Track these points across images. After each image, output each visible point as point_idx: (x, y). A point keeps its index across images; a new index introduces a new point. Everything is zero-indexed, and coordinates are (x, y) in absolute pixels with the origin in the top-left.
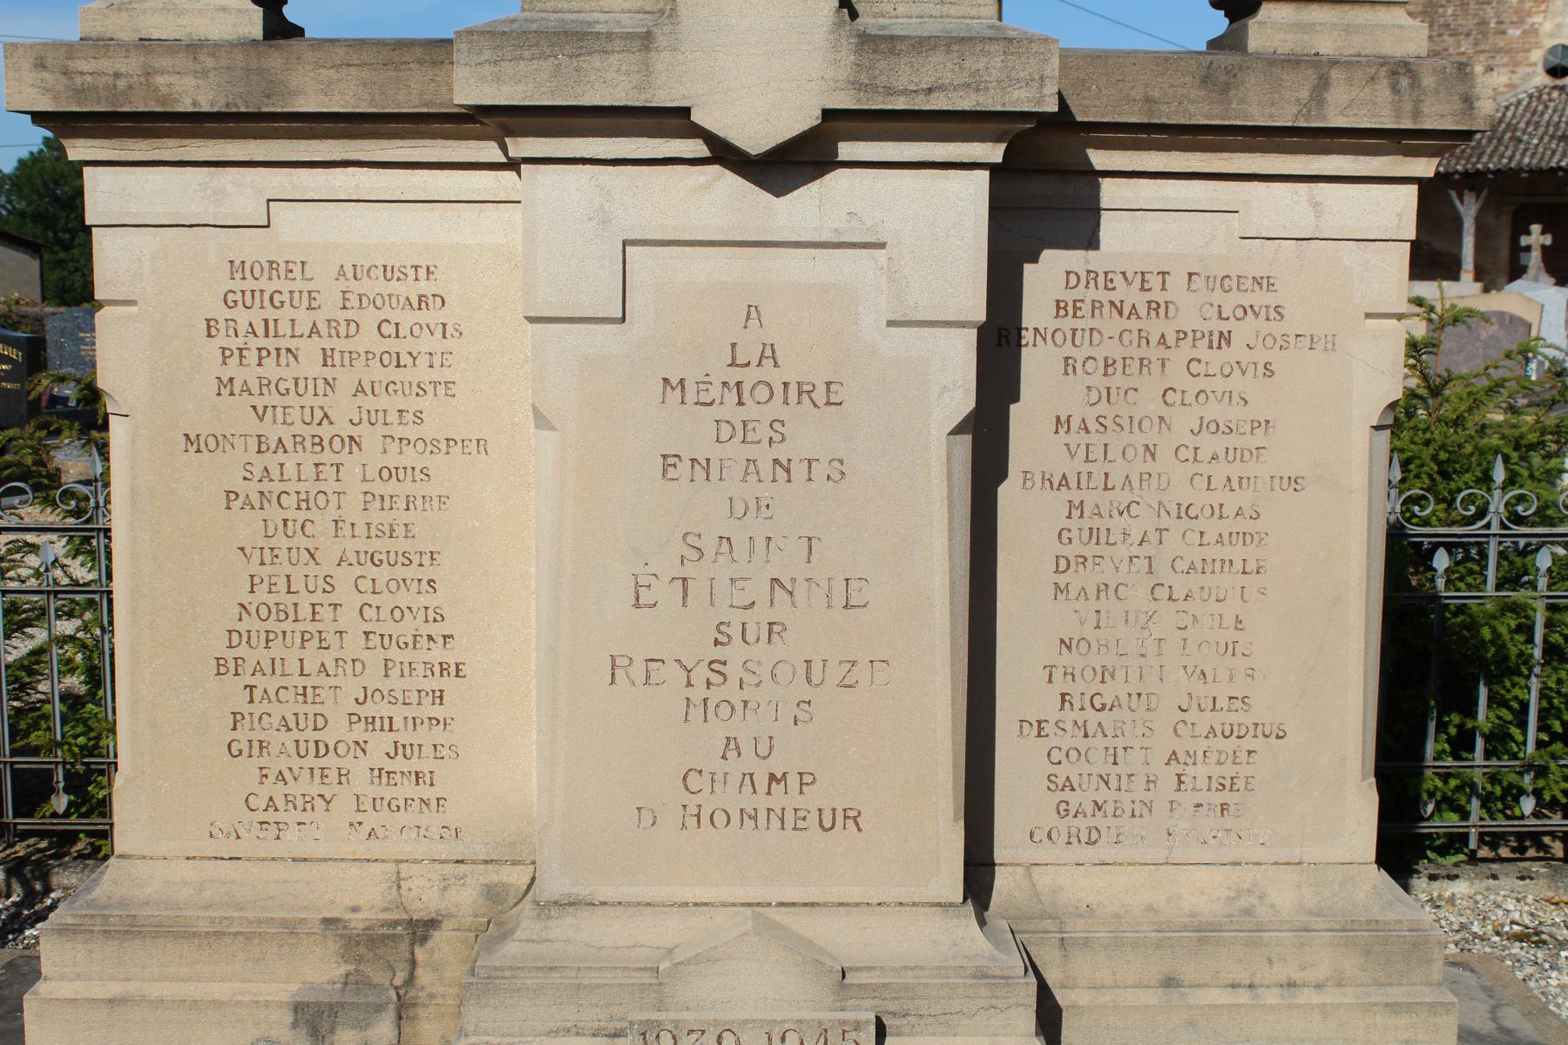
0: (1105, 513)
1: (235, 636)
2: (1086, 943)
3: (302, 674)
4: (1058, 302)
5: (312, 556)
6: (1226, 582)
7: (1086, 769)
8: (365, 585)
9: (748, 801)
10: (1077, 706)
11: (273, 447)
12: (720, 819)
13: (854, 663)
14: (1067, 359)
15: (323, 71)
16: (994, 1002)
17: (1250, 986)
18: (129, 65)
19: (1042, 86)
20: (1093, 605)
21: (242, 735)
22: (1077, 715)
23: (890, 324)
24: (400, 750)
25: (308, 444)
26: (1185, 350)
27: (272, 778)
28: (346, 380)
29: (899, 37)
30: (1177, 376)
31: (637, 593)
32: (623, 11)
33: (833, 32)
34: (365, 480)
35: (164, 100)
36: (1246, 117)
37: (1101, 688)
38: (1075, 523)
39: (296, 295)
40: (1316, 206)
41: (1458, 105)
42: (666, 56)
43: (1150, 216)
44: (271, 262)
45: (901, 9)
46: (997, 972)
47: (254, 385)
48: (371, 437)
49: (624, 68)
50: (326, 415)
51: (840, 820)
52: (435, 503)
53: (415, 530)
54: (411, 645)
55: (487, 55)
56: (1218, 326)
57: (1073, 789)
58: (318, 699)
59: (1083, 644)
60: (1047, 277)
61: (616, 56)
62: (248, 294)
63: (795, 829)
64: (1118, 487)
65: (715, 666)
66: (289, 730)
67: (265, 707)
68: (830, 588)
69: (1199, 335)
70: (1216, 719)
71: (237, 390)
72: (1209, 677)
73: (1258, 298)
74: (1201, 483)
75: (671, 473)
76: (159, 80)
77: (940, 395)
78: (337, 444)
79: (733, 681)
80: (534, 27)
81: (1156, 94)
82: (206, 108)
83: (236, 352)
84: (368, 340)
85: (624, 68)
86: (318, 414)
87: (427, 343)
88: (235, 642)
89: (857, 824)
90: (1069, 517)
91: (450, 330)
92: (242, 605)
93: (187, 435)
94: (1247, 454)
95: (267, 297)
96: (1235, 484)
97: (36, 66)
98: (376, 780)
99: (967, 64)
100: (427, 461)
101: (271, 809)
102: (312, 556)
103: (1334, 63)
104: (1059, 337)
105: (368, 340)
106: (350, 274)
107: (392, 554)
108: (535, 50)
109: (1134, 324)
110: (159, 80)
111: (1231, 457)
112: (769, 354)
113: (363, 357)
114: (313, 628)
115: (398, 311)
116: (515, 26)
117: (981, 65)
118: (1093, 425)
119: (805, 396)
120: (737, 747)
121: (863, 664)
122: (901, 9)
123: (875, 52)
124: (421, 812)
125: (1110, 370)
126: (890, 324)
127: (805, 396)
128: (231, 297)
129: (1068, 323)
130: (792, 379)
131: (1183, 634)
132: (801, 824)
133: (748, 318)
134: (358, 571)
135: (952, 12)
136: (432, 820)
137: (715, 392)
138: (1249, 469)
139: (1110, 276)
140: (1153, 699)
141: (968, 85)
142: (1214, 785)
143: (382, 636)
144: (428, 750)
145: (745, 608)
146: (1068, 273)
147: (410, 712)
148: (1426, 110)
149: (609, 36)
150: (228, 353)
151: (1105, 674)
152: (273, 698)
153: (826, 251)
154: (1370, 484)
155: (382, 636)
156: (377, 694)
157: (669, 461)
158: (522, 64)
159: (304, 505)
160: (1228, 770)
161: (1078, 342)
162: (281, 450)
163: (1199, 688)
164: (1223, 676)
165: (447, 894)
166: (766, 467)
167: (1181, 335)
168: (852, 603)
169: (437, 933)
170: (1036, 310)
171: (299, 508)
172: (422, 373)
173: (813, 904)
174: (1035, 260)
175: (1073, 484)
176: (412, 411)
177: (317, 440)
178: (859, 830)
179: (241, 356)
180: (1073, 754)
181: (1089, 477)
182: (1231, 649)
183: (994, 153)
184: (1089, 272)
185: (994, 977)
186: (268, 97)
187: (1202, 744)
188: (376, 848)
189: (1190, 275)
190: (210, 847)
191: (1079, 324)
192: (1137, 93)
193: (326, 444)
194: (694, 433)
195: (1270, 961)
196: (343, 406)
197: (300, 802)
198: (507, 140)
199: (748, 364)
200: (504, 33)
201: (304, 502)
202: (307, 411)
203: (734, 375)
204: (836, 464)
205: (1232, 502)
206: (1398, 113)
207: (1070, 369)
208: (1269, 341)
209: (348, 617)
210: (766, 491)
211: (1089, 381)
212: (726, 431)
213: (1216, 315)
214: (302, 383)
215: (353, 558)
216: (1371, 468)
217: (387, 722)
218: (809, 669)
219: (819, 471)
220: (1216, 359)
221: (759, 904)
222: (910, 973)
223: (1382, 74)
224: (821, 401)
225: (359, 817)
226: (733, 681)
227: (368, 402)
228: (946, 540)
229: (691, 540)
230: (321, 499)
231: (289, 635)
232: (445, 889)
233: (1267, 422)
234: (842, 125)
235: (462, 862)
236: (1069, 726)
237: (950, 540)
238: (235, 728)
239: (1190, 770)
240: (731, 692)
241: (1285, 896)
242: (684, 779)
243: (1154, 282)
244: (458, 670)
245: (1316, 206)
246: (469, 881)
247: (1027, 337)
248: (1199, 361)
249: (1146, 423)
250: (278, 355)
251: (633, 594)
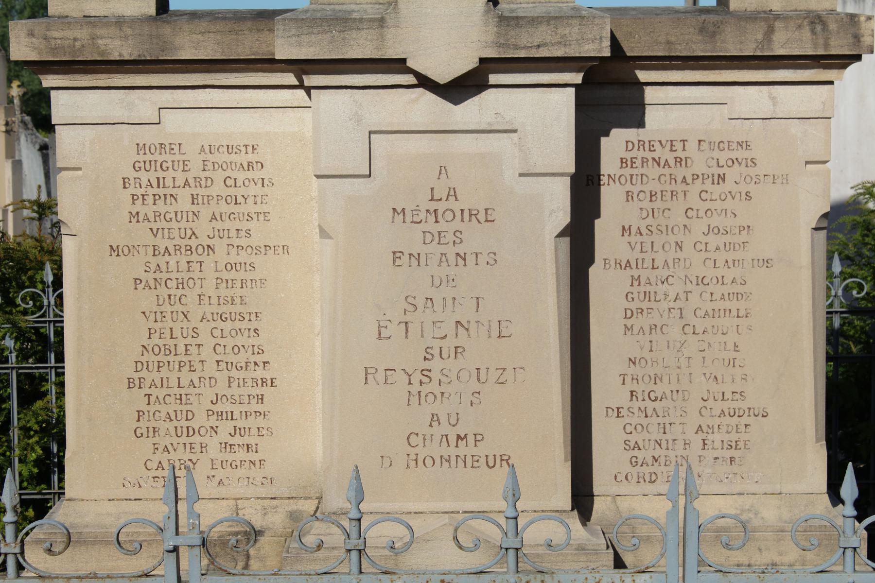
0: (653, 283)
1: (139, 365)
4: (622, 159)
5: (186, 316)
7: (647, 436)
8: (217, 333)
9: (445, 451)
10: (640, 398)
11: (162, 252)
12: (429, 462)
13: (504, 370)
14: (628, 192)
15: (194, 35)
17: (749, 566)
18: (82, 34)
19: (601, 42)
20: (648, 337)
21: (143, 424)
22: (640, 404)
23: (521, 175)
24: (238, 431)
25: (183, 250)
26: (698, 186)
27: (161, 450)
28: (206, 213)
29: (521, 17)
30: (693, 200)
31: (379, 331)
32: (367, 4)
33: (484, 16)
34: (216, 271)
35: (103, 53)
36: (726, 51)
37: (654, 388)
38: (635, 289)
39: (176, 163)
40: (774, 100)
41: (851, 40)
42: (392, 30)
43: (673, 108)
44: (161, 144)
46: (590, 547)
47: (151, 216)
48: (220, 246)
50: (194, 233)
53: (247, 300)
54: (244, 368)
55: (293, 31)
56: (718, 171)
57: (640, 449)
58: (188, 402)
59: (643, 362)
60: (615, 145)
61: (365, 31)
62: (148, 163)
63: (472, 467)
64: (661, 267)
65: (425, 373)
66: (171, 420)
67: (157, 407)
69: (706, 176)
70: (725, 406)
71: (141, 219)
72: (720, 380)
73: (741, 154)
74: (710, 263)
75: (398, 262)
76: (100, 42)
77: (550, 214)
80: (319, 15)
81: (673, 39)
82: (127, 58)
83: (141, 197)
84: (218, 189)
86: (189, 232)
87: (253, 190)
90: (632, 285)
92: (144, 346)
93: (111, 246)
95: (158, 165)
96: (730, 264)
97: (28, 35)
98: (223, 450)
99: (559, 31)
100: (253, 259)
101: (160, 469)
102: (186, 316)
103: (777, 17)
104: (623, 180)
106: (207, 151)
107: (233, 314)
108: (320, 29)
109: (667, 171)
110: (100, 42)
111: (727, 248)
112: (453, 194)
113: (215, 198)
114: (186, 359)
115: (236, 172)
116: (308, 15)
117: (567, 32)
118: (644, 231)
119: (473, 217)
120: (438, 420)
123: (508, 25)
126: (521, 175)
127: (473, 217)
128: (137, 165)
129: (628, 171)
131: (703, 354)
132: (476, 464)
133: (440, 173)
134: (213, 324)
136: (257, 474)
137: (422, 216)
138: (738, 255)
139: (652, 143)
140: (686, 393)
141: (560, 43)
142: (726, 446)
143: (227, 363)
144: (254, 431)
145: (442, 338)
146: (627, 142)
147: (244, 408)
148: (832, 43)
149: (361, 20)
150: (135, 197)
152: (162, 401)
154: (813, 263)
155: (227, 363)
157: (396, 255)
158: (313, 36)
159: (180, 286)
160: (734, 437)
161: (634, 182)
162: (167, 254)
163: (716, 388)
164: (728, 379)
165: (266, 517)
166: (452, 258)
167: (695, 177)
168: (502, 334)
169: (262, 538)
170: (609, 164)
174: (607, 135)
176: (244, 230)
177: (188, 248)
179: (144, 199)
180: (639, 428)
182: (732, 362)
183: (577, 78)
184: (639, 141)
186: (163, 51)
187: (717, 421)
188: (223, 492)
189: (700, 141)
190: (122, 493)
191: (634, 172)
192: (662, 39)
193: (193, 250)
194: (411, 239)
195: (760, 550)
196: (203, 228)
198: (304, 77)
199: (441, 200)
200: (303, 19)
201: (181, 284)
202: (183, 231)
203: (433, 206)
204: (492, 255)
206: (815, 46)
207: (630, 198)
208: (748, 179)
209: (206, 352)
210: (452, 271)
211: (641, 205)
212: (429, 237)
213: (716, 164)
215: (210, 317)
216: (813, 253)
217: (230, 414)
218: (478, 373)
219: (482, 259)
220: (716, 190)
221: (452, 512)
223: (805, 23)
224: (482, 219)
225: (213, 473)
227: (219, 225)
229: (410, 300)
230: (191, 282)
231: (171, 363)
232: (265, 514)
233: (749, 227)
235: (274, 498)
236: (636, 410)
238: (139, 420)
239: (710, 437)
240: (434, 387)
241: (770, 513)
242: (408, 439)
243: (679, 146)
244: (272, 382)
245: (774, 100)
246: (279, 510)
247: (604, 180)
248: (707, 192)
249: (676, 229)
250: (165, 198)
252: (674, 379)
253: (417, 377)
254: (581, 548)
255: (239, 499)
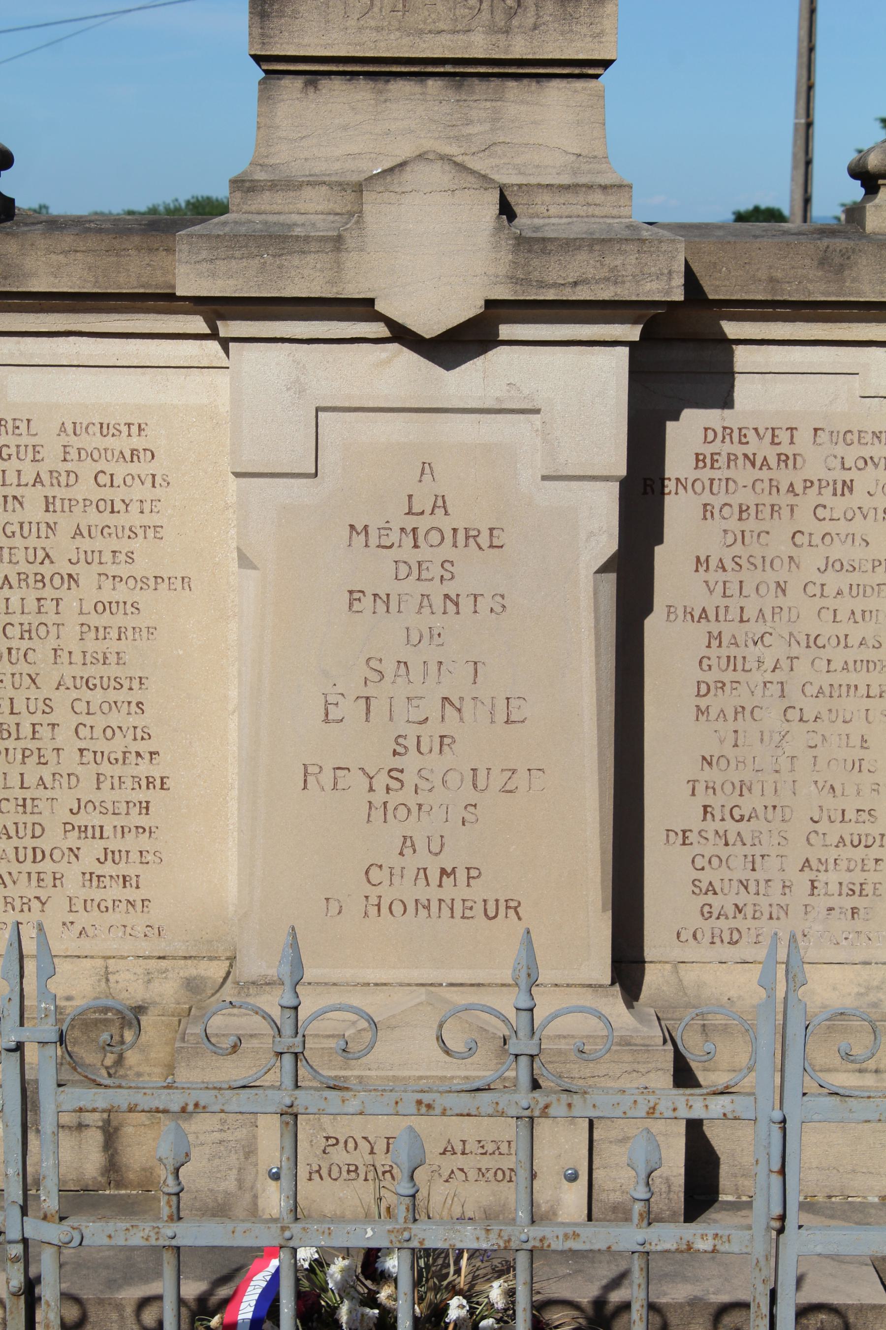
2: (725, 1029)
3: (22, 787)
4: (697, 455)
5: (33, 681)
6: (851, 705)
8: (81, 707)
9: (422, 892)
10: (718, 817)
12: (398, 908)
13: (514, 771)
14: (705, 505)
15: (53, 256)
16: (636, 1066)
20: (731, 725)
23: (545, 478)
25: (31, 580)
26: (813, 497)
28: (66, 524)
30: (804, 519)
33: (494, 235)
34: (81, 613)
36: (859, 294)
37: (739, 801)
38: (714, 652)
39: (22, 449)
43: (778, 379)
45: (553, 210)
48: (87, 575)
49: (318, 266)
50: (47, 556)
51: (502, 909)
52: (144, 633)
53: (126, 658)
54: (121, 761)
55: (204, 254)
57: (715, 893)
58: (36, 810)
59: (723, 761)
60: (687, 434)
61: (313, 256)
63: (463, 917)
64: (753, 620)
65: (393, 774)
66: (10, 837)
68: (493, 705)
69: (824, 484)
70: (846, 830)
72: (838, 791)
74: (828, 615)
78: (57, 581)
79: (409, 787)
80: (243, 230)
81: (779, 275)
84: (85, 489)
85: (318, 266)
86: (41, 554)
87: (138, 492)
88: (403, 573)
89: (517, 913)
90: (709, 646)
91: (158, 480)
94: (869, 590)
96: (858, 616)
98: (87, 883)
99: (607, 261)
100: (137, 596)
102: (33, 681)
104: (698, 487)
105: (85, 489)
107: (105, 679)
109: (765, 474)
111: (854, 593)
112: (441, 504)
113: (81, 504)
114: (32, 745)
115: (113, 463)
117: (618, 262)
118: (729, 564)
119: (471, 540)
120: (413, 845)
121: (522, 773)
122: (553, 210)
123: (529, 251)
124: (127, 912)
125: (745, 515)
126: (545, 478)
127: (471, 540)
129: (706, 474)
130: (461, 526)
131: (814, 752)
132: (468, 913)
133: (422, 473)
134: (75, 694)
135: (596, 213)
136: (137, 920)
137: (395, 537)
140: (787, 810)
141: (607, 279)
142: (845, 890)
143: (95, 753)
144: (134, 856)
145: (420, 723)
146: (706, 429)
147: (119, 821)
149: (307, 239)
151: (743, 788)
153: (489, 416)
155: (95, 753)
156: (90, 805)
157: (354, 596)
159: (26, 635)
160: (858, 877)
161: (715, 490)
163: (830, 802)
165: (151, 986)
166: (438, 601)
167: (808, 484)
168: (512, 718)
170: (678, 460)
171: (22, 638)
172: (134, 518)
173: (479, 985)
175: (712, 617)
176: (124, 552)
177: (39, 577)
178: (519, 918)
180: (715, 861)
181: (727, 611)
182: (858, 766)
183: (633, 332)
184: (724, 428)
185: (636, 1045)
186: (5, 278)
187: (833, 853)
188: (86, 946)
189: (816, 430)
191: (716, 474)
192: (763, 274)
194: (377, 571)
196: (63, 546)
197: (18, 904)
198: (219, 323)
199: (422, 513)
201: (27, 633)
202: (31, 551)
203: (410, 522)
204: (498, 598)
205: (856, 633)
207: (708, 514)
209: (64, 736)
210: (437, 622)
211: (725, 525)
212: (403, 570)
213: (839, 466)
214: (26, 527)
215: (69, 683)
217: (98, 830)
218: (475, 776)
221: (431, 985)
222: (563, 1041)
225: (71, 917)
226: (409, 787)
227: (86, 544)
228: (593, 664)
229: (373, 664)
231: (11, 752)
232: (149, 981)
234: (503, 312)
235: (164, 958)
236: (711, 835)
237: (597, 663)
239: (822, 877)
240: (407, 796)
242: (367, 873)
244: (162, 783)
246: (170, 975)
247: (670, 486)
248: (825, 507)
249: (777, 563)
251: (323, 711)
252: (769, 789)
253: (381, 781)
254: (625, 1042)
255: (109, 958)
